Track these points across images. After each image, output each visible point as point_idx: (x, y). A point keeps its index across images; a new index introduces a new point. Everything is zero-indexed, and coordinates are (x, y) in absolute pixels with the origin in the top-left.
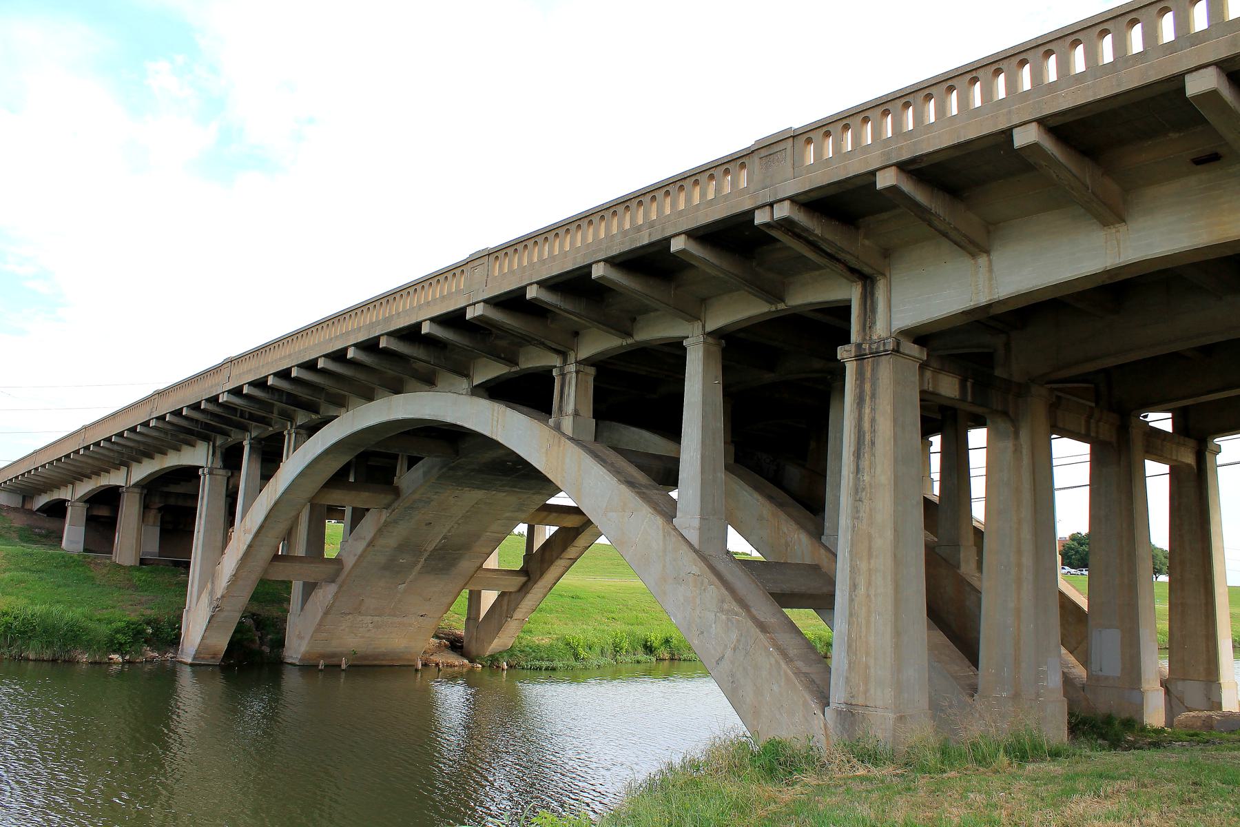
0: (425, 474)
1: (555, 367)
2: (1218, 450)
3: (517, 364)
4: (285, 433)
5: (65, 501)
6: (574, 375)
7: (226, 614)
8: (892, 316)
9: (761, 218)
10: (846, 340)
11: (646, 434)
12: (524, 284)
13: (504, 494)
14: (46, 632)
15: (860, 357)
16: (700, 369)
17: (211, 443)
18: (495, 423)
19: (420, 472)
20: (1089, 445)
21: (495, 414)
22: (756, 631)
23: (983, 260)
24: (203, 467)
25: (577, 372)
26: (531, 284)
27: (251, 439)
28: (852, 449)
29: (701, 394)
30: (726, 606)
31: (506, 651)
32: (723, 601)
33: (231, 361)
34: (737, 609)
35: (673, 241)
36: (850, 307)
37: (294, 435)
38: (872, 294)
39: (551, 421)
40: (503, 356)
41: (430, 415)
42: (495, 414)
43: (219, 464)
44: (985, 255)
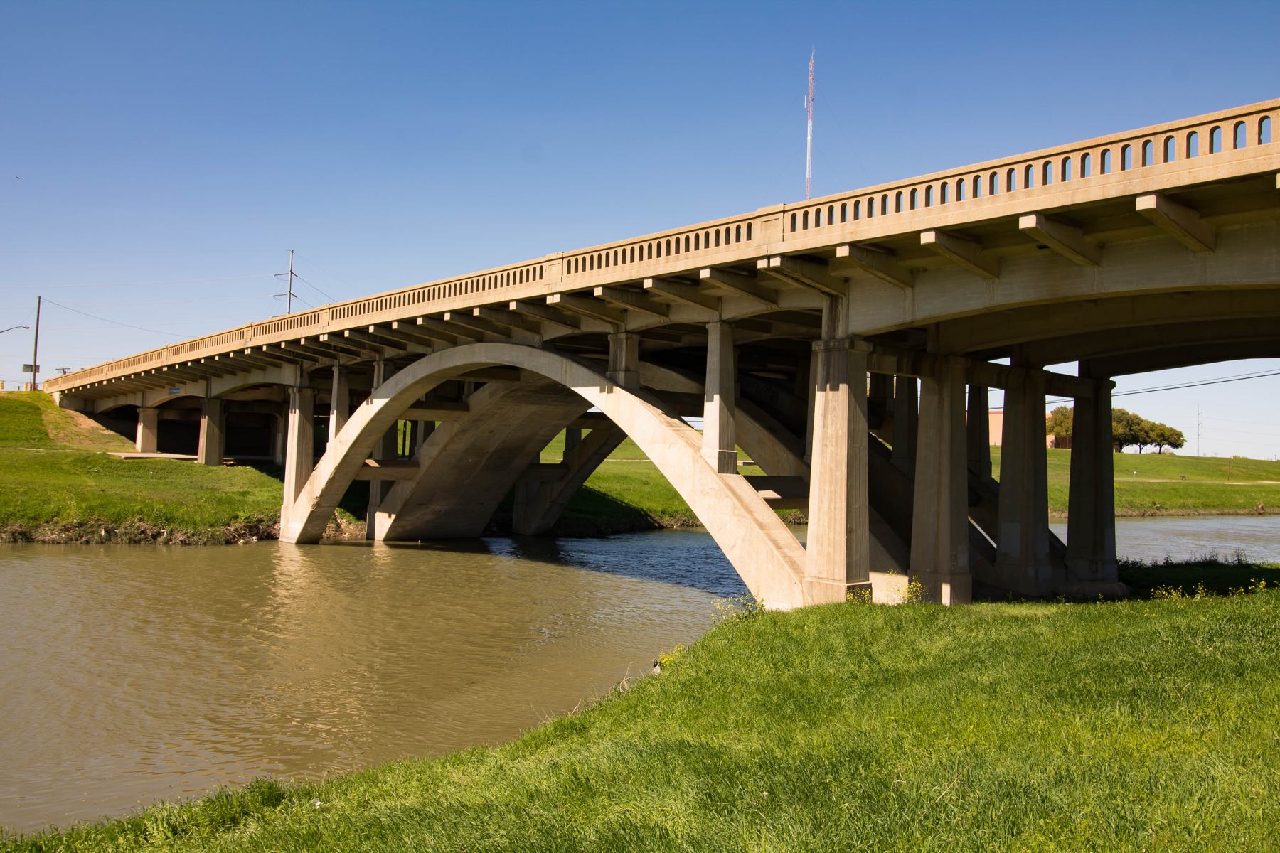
0: (491, 395)
1: (610, 333)
2: (1113, 384)
3: (580, 328)
4: (375, 363)
5: (136, 407)
6: (625, 340)
7: (323, 509)
8: (850, 323)
9: (762, 264)
10: (819, 337)
11: (674, 375)
12: (592, 285)
13: (553, 407)
14: (373, 538)
15: (828, 350)
16: (718, 346)
17: (298, 366)
18: (564, 373)
19: (487, 393)
20: (1003, 391)
21: (564, 366)
22: (757, 529)
23: (909, 291)
24: (291, 386)
25: (627, 339)
26: (598, 286)
27: (340, 365)
28: (821, 412)
29: (718, 363)
30: (737, 512)
31: (1015, 617)
32: (735, 508)
33: (329, 308)
34: (746, 514)
35: (702, 272)
36: (820, 318)
37: (382, 366)
38: (837, 307)
39: (608, 374)
40: (568, 322)
41: (507, 361)
42: (564, 366)
43: (306, 382)
44: (910, 289)
